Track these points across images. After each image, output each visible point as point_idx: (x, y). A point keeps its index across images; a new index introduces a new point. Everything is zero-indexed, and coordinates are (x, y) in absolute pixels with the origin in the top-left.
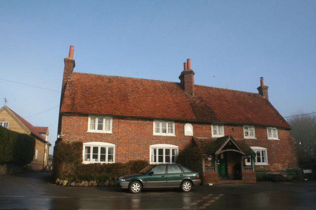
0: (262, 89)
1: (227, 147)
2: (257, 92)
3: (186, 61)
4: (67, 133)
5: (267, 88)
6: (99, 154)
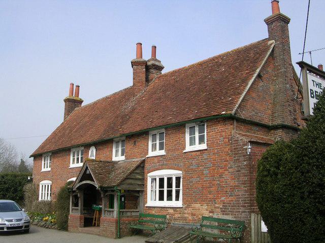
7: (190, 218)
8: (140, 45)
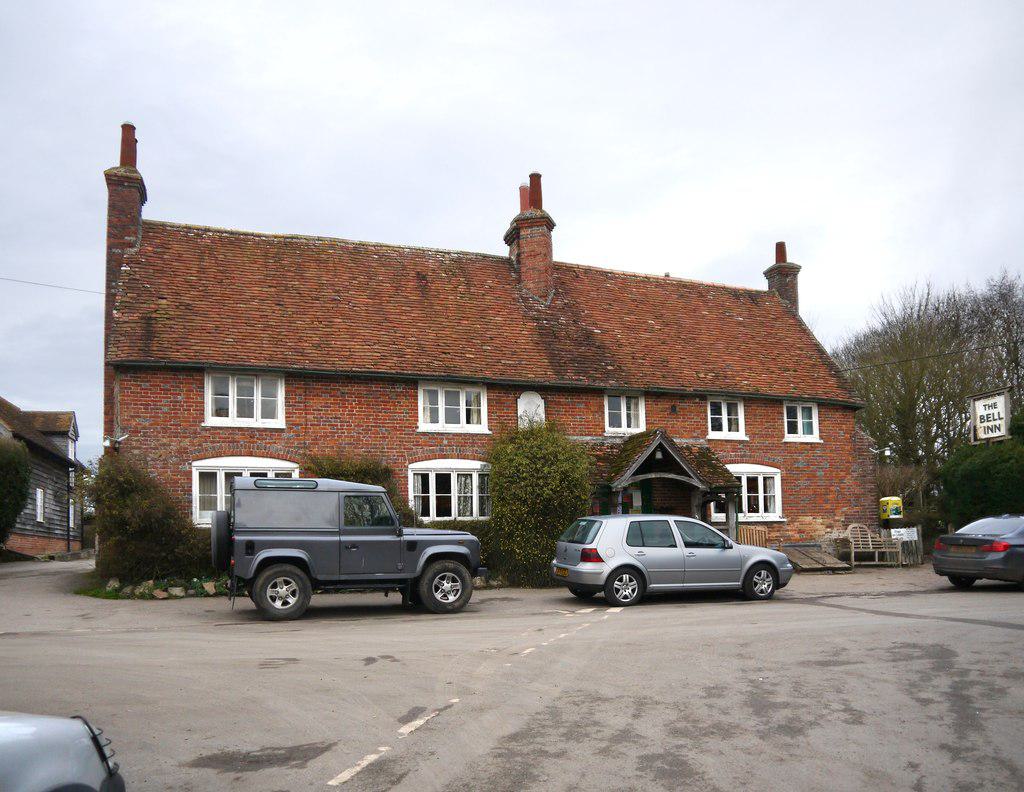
0: (783, 274)
1: (649, 465)
2: (762, 285)
3: (527, 182)
4: (136, 432)
5: (794, 270)
7: (797, 536)
8: (128, 131)
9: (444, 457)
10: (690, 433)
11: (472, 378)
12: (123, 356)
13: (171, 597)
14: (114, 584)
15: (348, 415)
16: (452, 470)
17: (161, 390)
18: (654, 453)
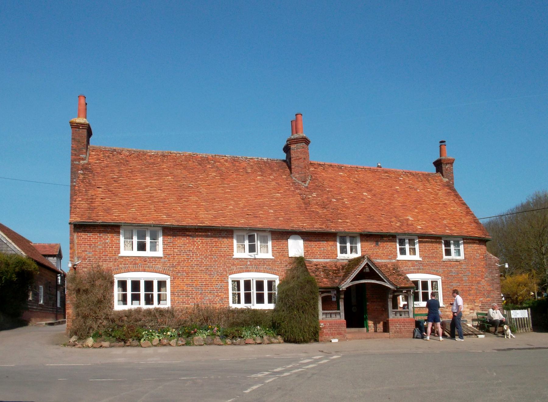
1: (361, 275)
4: (85, 259)
5: (451, 162)
6: (142, 292)
9: (248, 271)
10: (387, 256)
11: (262, 228)
12: (78, 220)
13: (226, 344)
14: (74, 339)
15: (196, 249)
16: (264, 278)
17: (98, 237)
18: (364, 268)
